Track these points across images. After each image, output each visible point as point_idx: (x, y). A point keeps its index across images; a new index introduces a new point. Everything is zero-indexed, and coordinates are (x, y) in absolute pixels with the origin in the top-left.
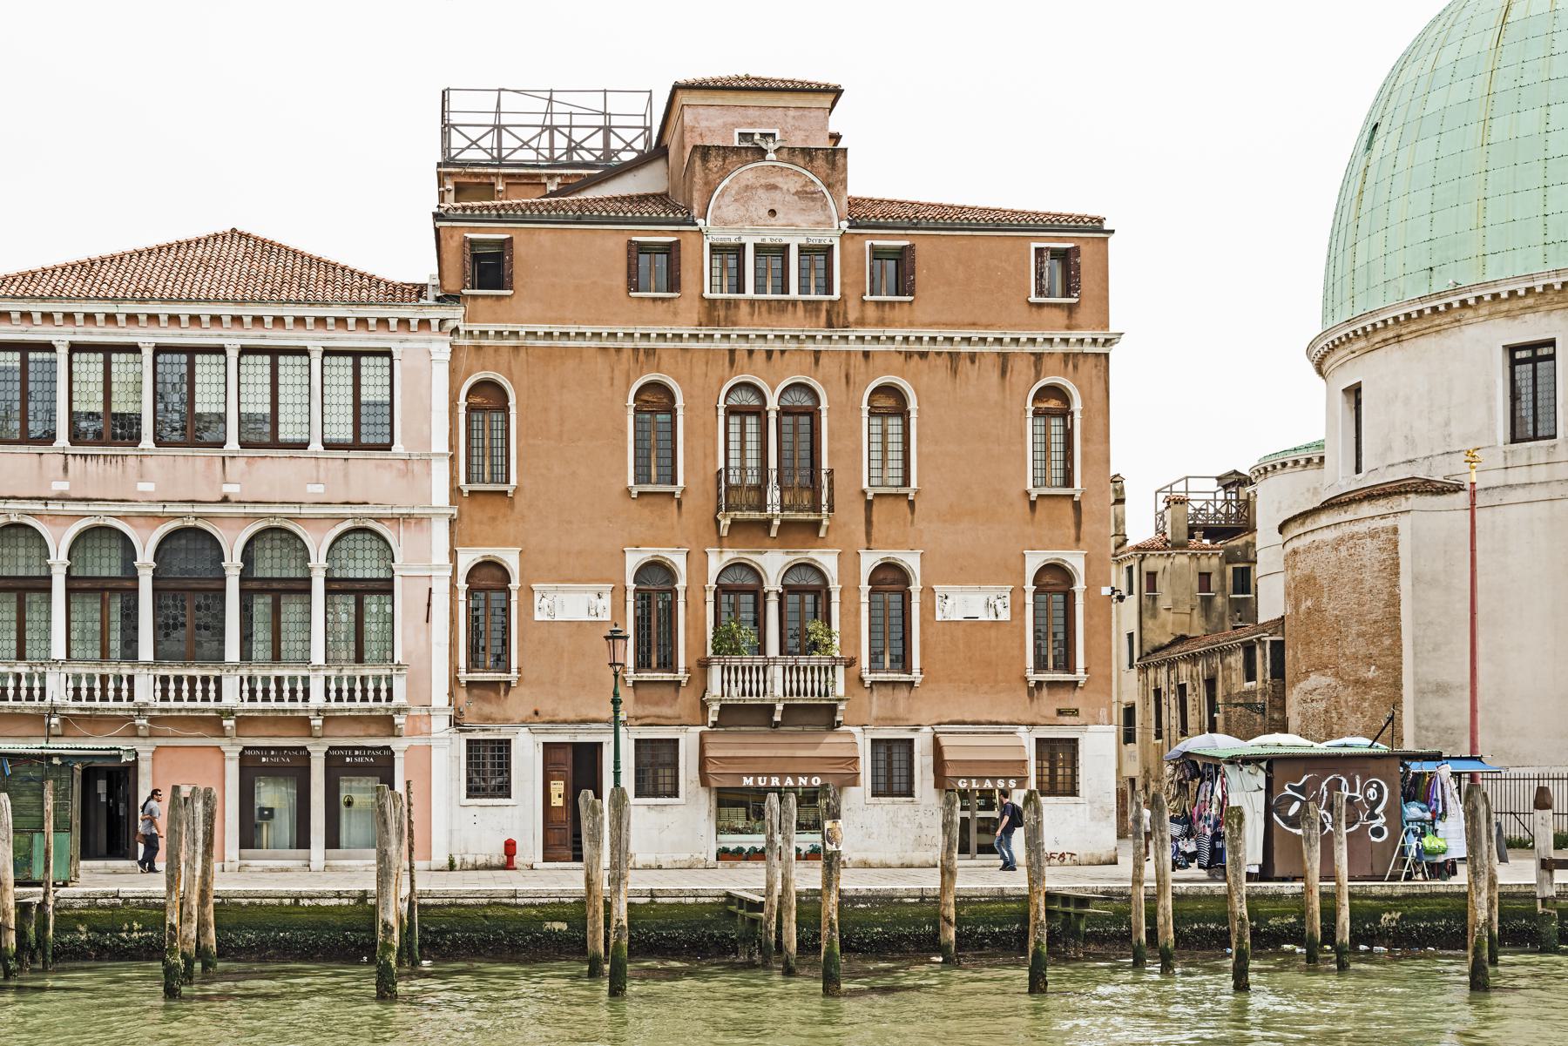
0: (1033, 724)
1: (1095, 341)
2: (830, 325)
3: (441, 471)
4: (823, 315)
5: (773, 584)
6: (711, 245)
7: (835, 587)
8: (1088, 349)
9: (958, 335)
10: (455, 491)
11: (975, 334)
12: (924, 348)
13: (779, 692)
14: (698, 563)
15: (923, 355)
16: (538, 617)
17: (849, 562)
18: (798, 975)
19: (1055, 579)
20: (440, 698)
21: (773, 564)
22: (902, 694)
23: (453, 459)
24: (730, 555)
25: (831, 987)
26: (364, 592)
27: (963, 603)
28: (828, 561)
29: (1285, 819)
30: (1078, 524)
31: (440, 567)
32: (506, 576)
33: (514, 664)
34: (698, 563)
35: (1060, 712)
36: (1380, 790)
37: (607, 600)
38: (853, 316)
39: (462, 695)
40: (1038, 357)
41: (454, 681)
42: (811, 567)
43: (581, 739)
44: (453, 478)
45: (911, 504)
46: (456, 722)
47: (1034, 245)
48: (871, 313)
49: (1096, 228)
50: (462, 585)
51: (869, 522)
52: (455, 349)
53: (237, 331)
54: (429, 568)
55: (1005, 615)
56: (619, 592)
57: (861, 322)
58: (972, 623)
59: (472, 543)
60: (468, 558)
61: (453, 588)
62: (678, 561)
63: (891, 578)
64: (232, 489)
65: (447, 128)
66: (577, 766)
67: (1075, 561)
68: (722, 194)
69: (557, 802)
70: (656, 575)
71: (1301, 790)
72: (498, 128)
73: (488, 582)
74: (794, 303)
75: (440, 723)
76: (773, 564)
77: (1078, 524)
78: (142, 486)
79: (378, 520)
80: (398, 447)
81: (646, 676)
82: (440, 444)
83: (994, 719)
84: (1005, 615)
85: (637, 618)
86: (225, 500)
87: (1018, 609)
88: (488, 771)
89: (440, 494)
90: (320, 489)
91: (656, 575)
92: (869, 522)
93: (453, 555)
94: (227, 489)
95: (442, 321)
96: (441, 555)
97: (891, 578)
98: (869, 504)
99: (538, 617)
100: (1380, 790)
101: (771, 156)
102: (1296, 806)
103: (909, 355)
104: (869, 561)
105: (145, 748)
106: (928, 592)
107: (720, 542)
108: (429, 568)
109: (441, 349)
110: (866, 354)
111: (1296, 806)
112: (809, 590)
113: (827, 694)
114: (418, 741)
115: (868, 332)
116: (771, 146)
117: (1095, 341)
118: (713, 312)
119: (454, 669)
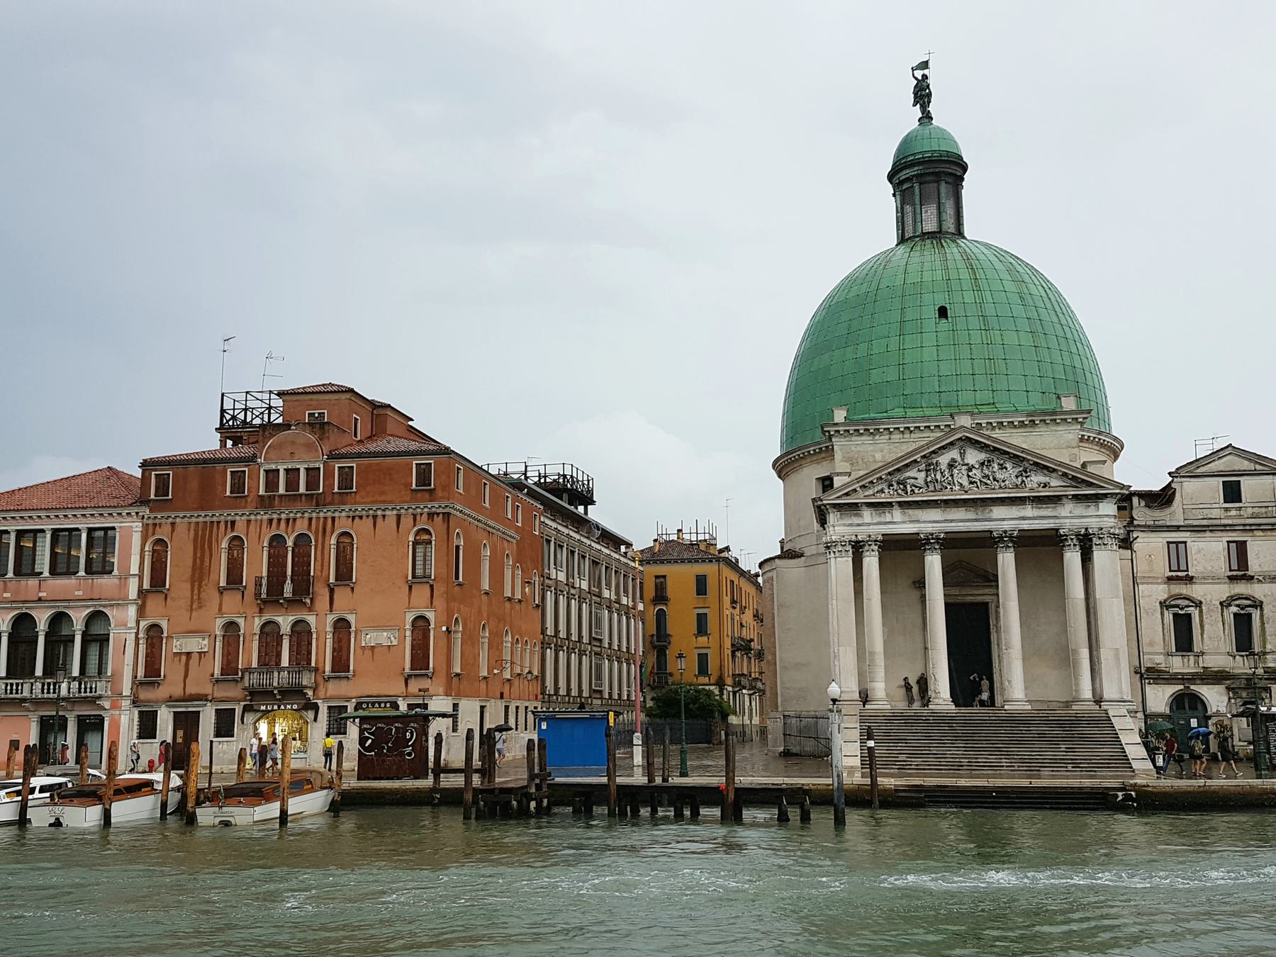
6: (1245, 542)
7: (313, 630)
13: (275, 684)
20: (126, 691)
21: (285, 622)
25: (467, 817)
26: (96, 639)
28: (311, 619)
33: (431, 666)
36: (412, 734)
38: (329, 499)
44: (141, 585)
53: (84, 520)
61: (137, 639)
62: (241, 622)
63: (342, 626)
65: (223, 411)
66: (187, 723)
69: (179, 740)
72: (246, 410)
74: (301, 495)
75: (126, 703)
76: (285, 622)
78: (5, 595)
80: (116, 572)
82: (134, 569)
83: (375, 693)
85: (334, 650)
86: (40, 599)
88: (147, 728)
89: (133, 593)
91: (231, 626)
93: (138, 622)
94: (41, 594)
98: (410, 587)
108: (125, 626)
109: (137, 526)
112: (301, 633)
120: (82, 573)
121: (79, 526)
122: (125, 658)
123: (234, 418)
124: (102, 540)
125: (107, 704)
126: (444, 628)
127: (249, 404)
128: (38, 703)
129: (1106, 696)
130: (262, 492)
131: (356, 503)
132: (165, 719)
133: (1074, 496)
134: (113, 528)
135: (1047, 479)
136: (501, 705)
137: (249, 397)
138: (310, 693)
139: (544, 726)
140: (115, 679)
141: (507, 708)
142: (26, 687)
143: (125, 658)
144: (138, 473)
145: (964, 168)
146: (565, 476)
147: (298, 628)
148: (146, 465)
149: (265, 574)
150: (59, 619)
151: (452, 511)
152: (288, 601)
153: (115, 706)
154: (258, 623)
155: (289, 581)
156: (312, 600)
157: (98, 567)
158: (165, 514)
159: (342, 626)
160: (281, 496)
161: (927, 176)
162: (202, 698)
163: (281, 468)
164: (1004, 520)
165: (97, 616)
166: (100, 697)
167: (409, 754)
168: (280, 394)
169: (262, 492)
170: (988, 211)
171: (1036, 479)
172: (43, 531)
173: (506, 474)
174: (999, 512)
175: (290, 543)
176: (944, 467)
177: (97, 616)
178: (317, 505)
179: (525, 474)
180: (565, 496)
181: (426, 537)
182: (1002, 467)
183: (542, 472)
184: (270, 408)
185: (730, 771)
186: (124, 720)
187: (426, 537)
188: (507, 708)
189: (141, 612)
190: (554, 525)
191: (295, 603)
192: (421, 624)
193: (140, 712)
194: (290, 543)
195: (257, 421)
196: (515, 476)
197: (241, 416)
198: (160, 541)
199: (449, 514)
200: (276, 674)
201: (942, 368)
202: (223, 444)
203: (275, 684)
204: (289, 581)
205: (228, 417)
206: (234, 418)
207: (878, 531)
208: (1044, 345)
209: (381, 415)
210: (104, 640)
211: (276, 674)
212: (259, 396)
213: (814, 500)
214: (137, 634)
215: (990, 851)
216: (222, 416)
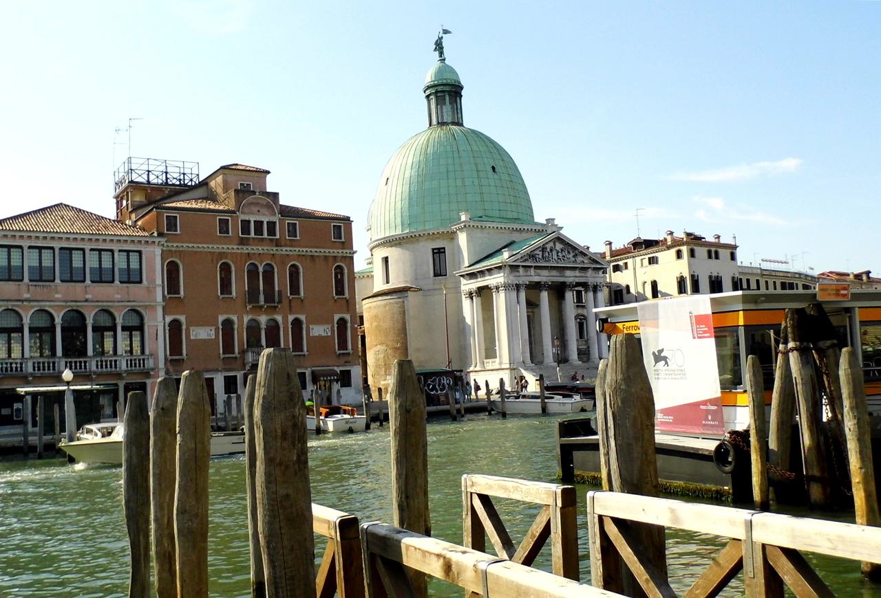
1: (299, 251)
2: (277, 246)
4: (275, 243)
8: (348, 255)
14: (241, 320)
21: (263, 319)
22: (302, 357)
23: (163, 287)
27: (318, 330)
28: (279, 318)
35: (346, 362)
37: (213, 332)
39: (168, 364)
40: (335, 257)
47: (287, 221)
48: (288, 243)
51: (290, 306)
52: (162, 250)
55: (329, 334)
57: (286, 246)
58: (320, 337)
59: (170, 314)
60: (169, 319)
62: (235, 318)
63: (297, 324)
64: (89, 296)
70: (228, 324)
76: (263, 319)
78: (57, 296)
84: (329, 334)
87: (333, 332)
90: (119, 296)
91: (228, 324)
93: (164, 319)
94: (87, 296)
100: (450, 381)
103: (299, 255)
104: (291, 318)
108: (157, 323)
109: (158, 251)
110: (288, 255)
113: (21, 370)
116: (257, 190)
129: (508, 372)
130: (240, 235)
133: (594, 268)
135: (582, 259)
145: (462, 88)
154: (246, 319)
155: (262, 294)
159: (297, 324)
161: (447, 93)
162: (217, 371)
164: (570, 277)
170: (475, 114)
171: (580, 259)
174: (568, 273)
175: (261, 269)
176: (548, 250)
182: (569, 252)
189: (165, 313)
194: (261, 269)
201: (459, 198)
204: (262, 294)
207: (526, 280)
208: (510, 190)
213: (732, 248)
215: (604, 454)
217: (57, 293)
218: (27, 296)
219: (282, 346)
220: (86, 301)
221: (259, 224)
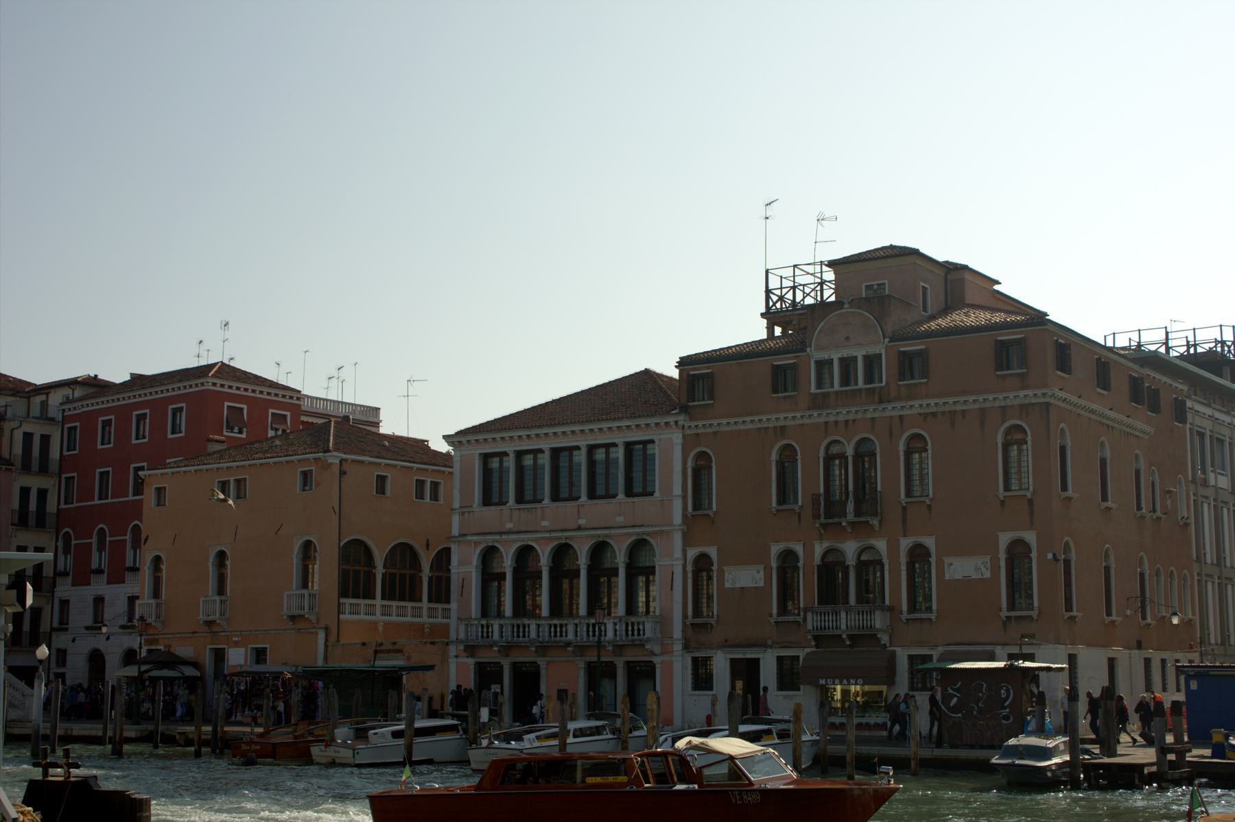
0: (1007, 644)
1: (921, 406)
3: (677, 506)
4: (877, 396)
5: (851, 561)
7: (886, 561)
8: (1034, 401)
9: (951, 400)
10: (684, 516)
11: (962, 399)
12: (934, 410)
13: (843, 627)
15: (934, 414)
16: (727, 585)
17: (893, 547)
18: (256, 764)
19: (1018, 551)
20: (677, 633)
21: (850, 549)
23: (684, 497)
24: (826, 544)
26: (639, 570)
27: (962, 568)
28: (881, 545)
29: (949, 708)
30: (1032, 513)
31: (677, 559)
32: (797, 559)
34: (893, 547)
36: (1008, 691)
41: (684, 624)
42: (871, 548)
43: (748, 656)
44: (685, 508)
45: (929, 507)
46: (686, 647)
49: (376, 410)
50: (689, 568)
51: (904, 520)
52: (684, 437)
54: (672, 559)
55: (987, 575)
56: (768, 570)
58: (967, 581)
60: (692, 553)
62: (799, 548)
63: (918, 554)
64: (582, 522)
65: (768, 292)
66: (746, 671)
67: (1030, 537)
68: (820, 331)
70: (788, 557)
71: (957, 690)
72: (794, 288)
73: (702, 563)
74: (860, 390)
75: (678, 647)
77: (1032, 513)
79: (648, 534)
80: (657, 494)
81: (1012, 614)
82: (677, 490)
84: (987, 575)
86: (579, 528)
87: (995, 569)
88: (702, 680)
91: (788, 557)
92: (904, 520)
95: (676, 422)
96: (678, 554)
97: (918, 554)
98: (904, 509)
99: (727, 585)
101: (846, 306)
102: (955, 700)
103: (926, 415)
104: (905, 543)
105: (542, 662)
106: (940, 563)
107: (821, 538)
108: (672, 559)
109: (677, 438)
111: (955, 700)
112: (868, 566)
114: (666, 658)
115: (898, 405)
117: (921, 406)
118: (819, 402)
119: (685, 616)
120: (547, 501)
121: (616, 441)
122: (669, 595)
123: (781, 298)
124: (637, 453)
125: (657, 649)
126: (1050, 556)
127: (799, 280)
128: (581, 649)
130: (813, 390)
131: (927, 396)
132: (721, 665)
134: (652, 442)
136: (1138, 656)
137: (798, 272)
138: (885, 639)
139: (1194, 685)
140: (664, 621)
141: (1147, 662)
142: (571, 629)
143: (669, 595)
144: (675, 374)
146: (1223, 343)
147: (830, 559)
148: (684, 363)
149: (822, 491)
150: (600, 549)
151: (1052, 401)
152: (852, 524)
153: (666, 651)
154: (819, 549)
156: (881, 522)
157: (638, 486)
158: (707, 422)
160: (837, 393)
162: (764, 645)
163: (232, 480)
165: (639, 546)
166: (648, 640)
167: (1006, 718)
168: (832, 264)
169: (813, 390)
172: (578, 448)
173: (1139, 345)
177: (639, 546)
178: (881, 402)
179: (1166, 343)
180: (1227, 371)
181: (1019, 436)
183: (1191, 339)
184: (822, 283)
185: (599, 656)
186: (677, 667)
187: (1019, 436)
188: (1147, 662)
189: (687, 542)
190: (1208, 411)
191: (860, 528)
192: (1018, 551)
193: (695, 660)
195: (809, 301)
196: (1153, 348)
197: (790, 296)
198: (702, 455)
199: (1048, 404)
200: (843, 615)
202: (770, 330)
203: (843, 627)
205: (775, 298)
206: (781, 298)
209: (957, 282)
210: (650, 571)
211: (843, 615)
212: (810, 269)
214: (684, 566)
216: (768, 298)
217: (543, 518)
218: (509, 526)
219: (887, 602)
220: (579, 528)
221: (847, 365)
